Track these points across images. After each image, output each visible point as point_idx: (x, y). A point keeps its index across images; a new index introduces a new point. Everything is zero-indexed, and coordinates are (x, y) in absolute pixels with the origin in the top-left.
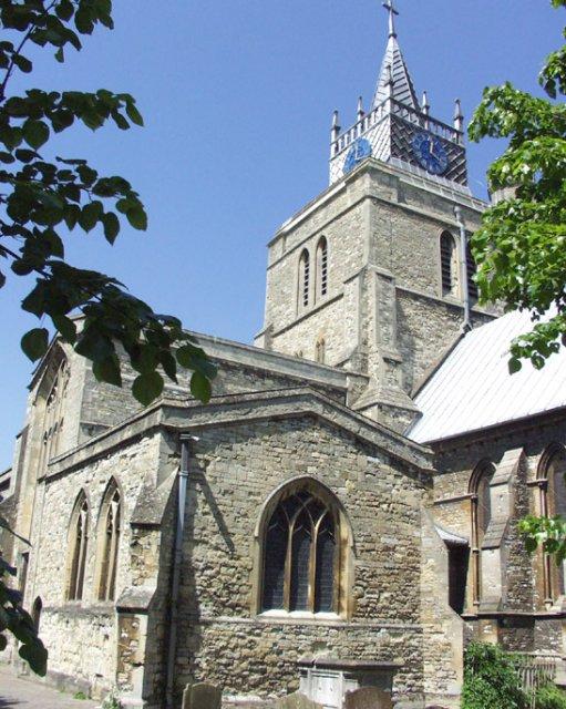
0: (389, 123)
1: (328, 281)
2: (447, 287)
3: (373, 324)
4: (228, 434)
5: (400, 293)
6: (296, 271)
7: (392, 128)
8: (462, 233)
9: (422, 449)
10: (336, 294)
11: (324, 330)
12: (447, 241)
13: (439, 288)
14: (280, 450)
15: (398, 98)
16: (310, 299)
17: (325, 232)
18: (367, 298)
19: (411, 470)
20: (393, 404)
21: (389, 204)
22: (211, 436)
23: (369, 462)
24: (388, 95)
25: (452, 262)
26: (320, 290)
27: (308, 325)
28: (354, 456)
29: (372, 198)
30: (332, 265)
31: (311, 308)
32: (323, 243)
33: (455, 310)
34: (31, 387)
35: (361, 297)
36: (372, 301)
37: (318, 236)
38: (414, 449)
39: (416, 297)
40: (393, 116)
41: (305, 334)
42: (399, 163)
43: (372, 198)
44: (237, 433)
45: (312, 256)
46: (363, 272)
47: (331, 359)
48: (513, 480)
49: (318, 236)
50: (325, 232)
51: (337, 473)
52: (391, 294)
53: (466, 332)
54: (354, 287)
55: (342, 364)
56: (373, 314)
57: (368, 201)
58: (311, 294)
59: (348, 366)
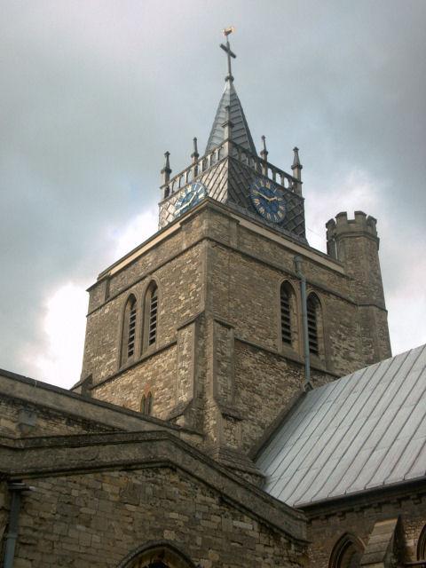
0: (227, 165)
1: (158, 328)
2: (287, 341)
3: (210, 373)
4: (70, 485)
5: (239, 343)
6: (120, 319)
7: (230, 171)
8: (304, 284)
9: (295, 514)
10: (167, 341)
11: (152, 382)
12: (286, 289)
13: (279, 341)
14: (132, 508)
15: (238, 142)
16: (136, 348)
17: (155, 276)
18: (204, 347)
19: (283, 540)
20: (232, 465)
21: (228, 248)
22: (49, 486)
23: (235, 527)
24: (226, 136)
25: (291, 313)
26: (147, 338)
27: (131, 378)
28: (218, 519)
29: (208, 239)
30: (163, 312)
31: (136, 358)
32: (153, 287)
33: (295, 364)
34: (161, 188)
35: (197, 345)
36: (210, 350)
37: (147, 280)
38: (284, 508)
39: (256, 349)
40: (231, 158)
41: (129, 387)
42: (232, 205)
43: (208, 239)
44: (81, 485)
45: (139, 304)
46: (199, 320)
47: (159, 412)
48: (388, 560)
49: (128, 292)
50: (155, 276)
51: (199, 541)
52: (229, 343)
53: (308, 390)
54: (188, 333)
55: (175, 419)
56: (210, 364)
57: (205, 244)
58: (137, 342)
59: (181, 421)
